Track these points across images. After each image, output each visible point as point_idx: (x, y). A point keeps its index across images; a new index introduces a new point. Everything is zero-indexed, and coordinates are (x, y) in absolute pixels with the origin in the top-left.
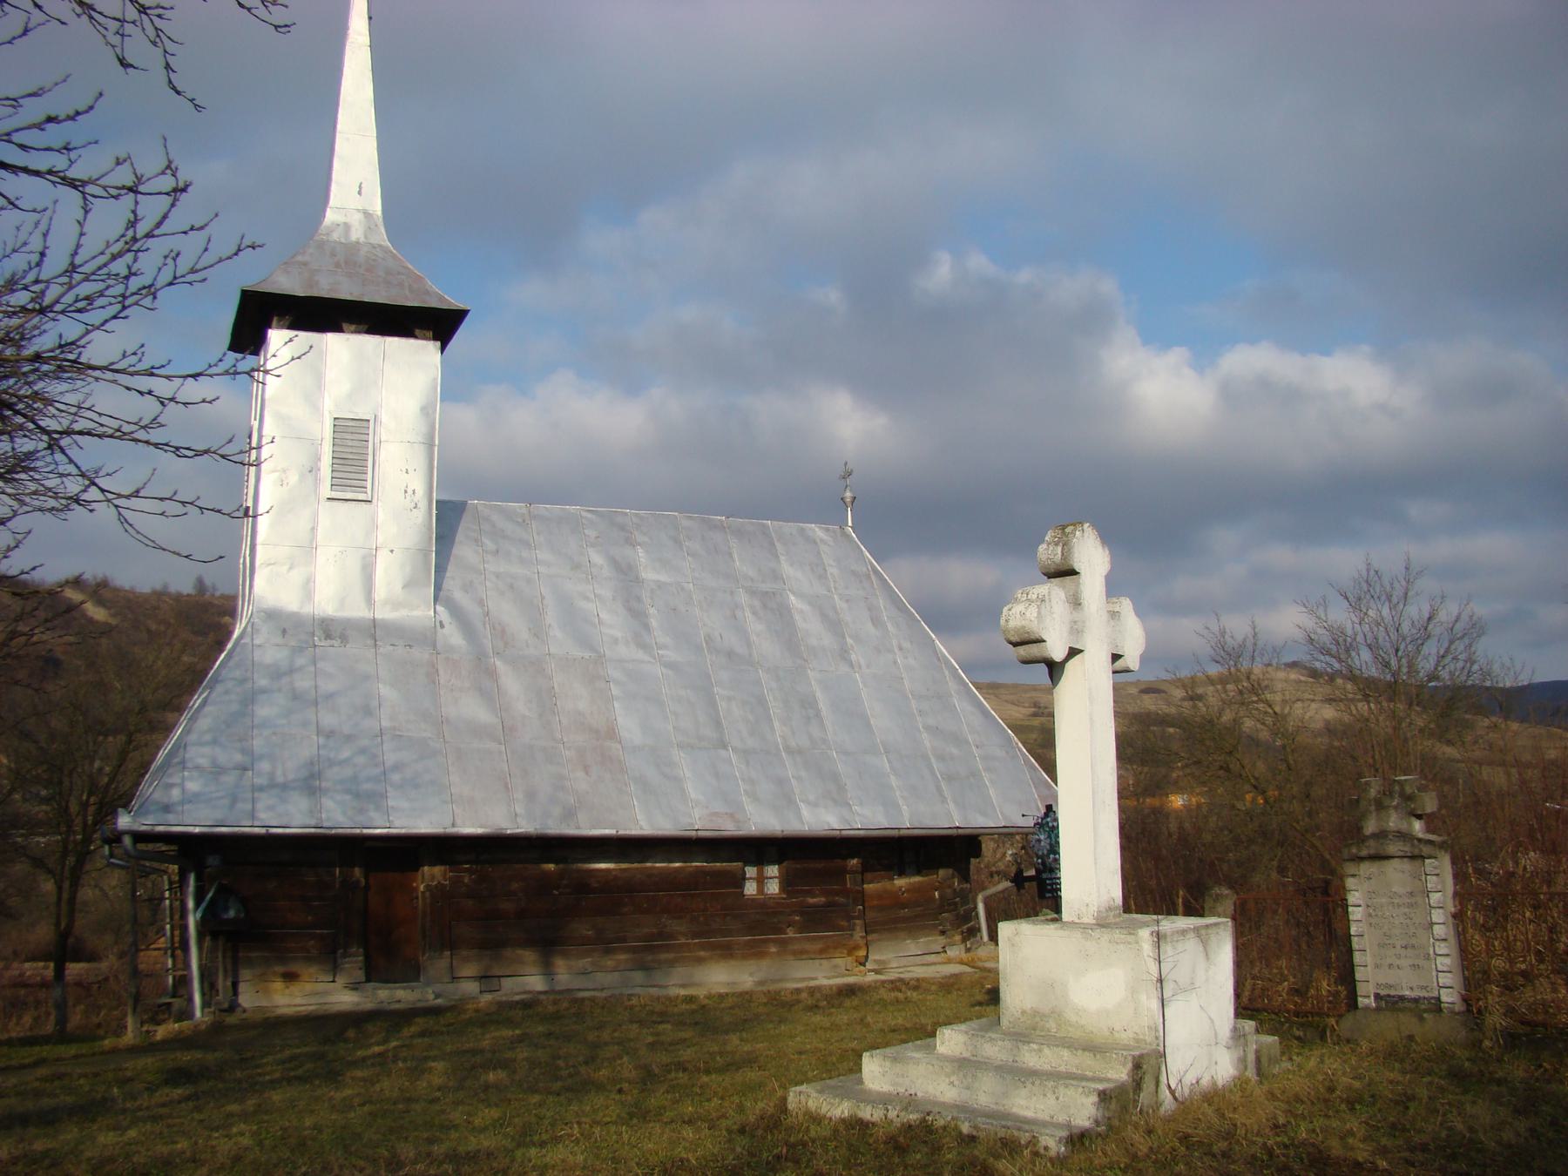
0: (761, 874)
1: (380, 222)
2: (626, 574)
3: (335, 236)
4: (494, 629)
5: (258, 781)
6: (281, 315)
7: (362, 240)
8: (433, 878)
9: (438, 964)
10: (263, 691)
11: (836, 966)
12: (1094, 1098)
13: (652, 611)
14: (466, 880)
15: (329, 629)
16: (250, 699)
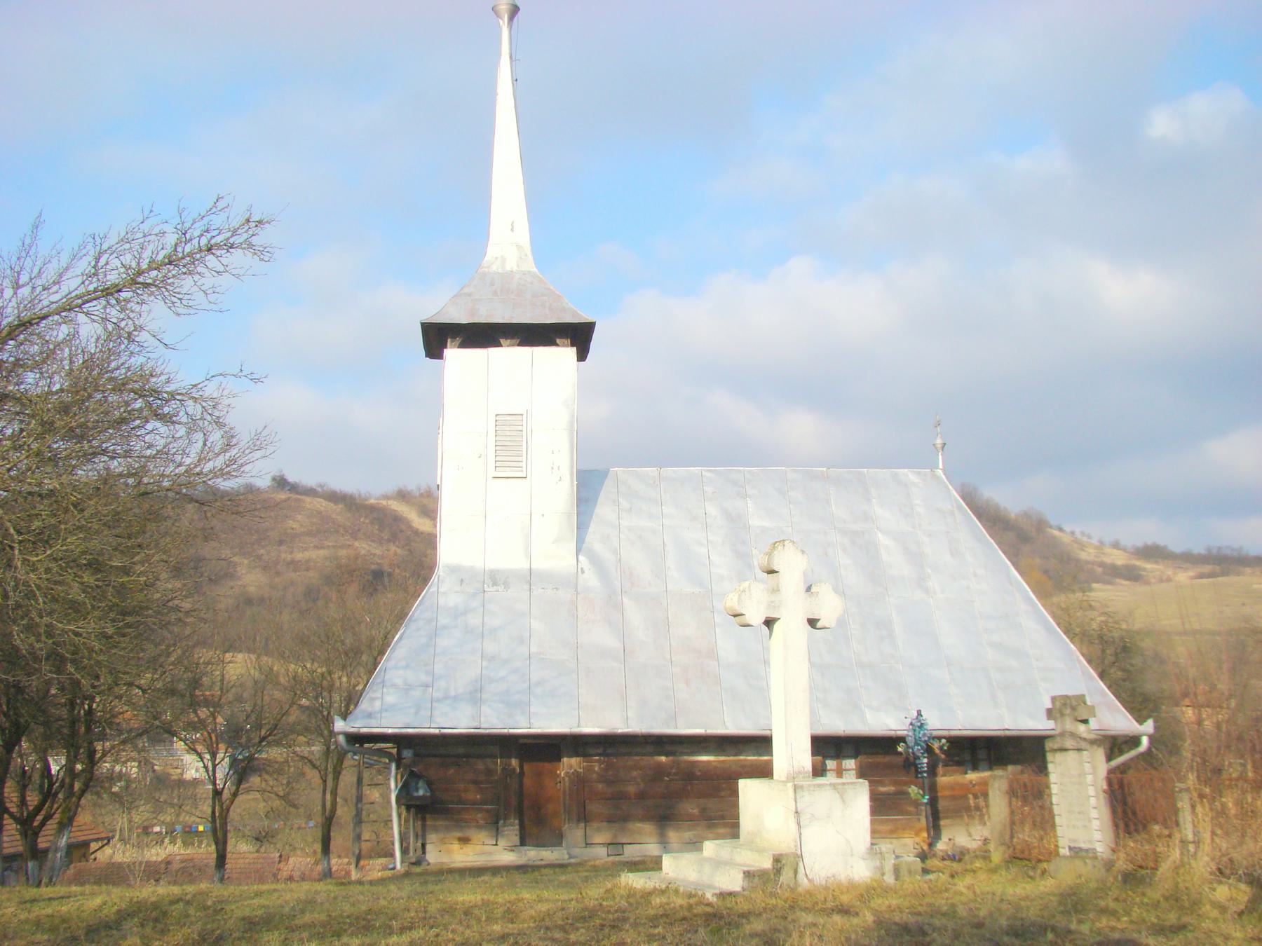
0: (839, 766)
1: (529, 252)
2: (736, 522)
3: (494, 268)
4: (624, 572)
5: (436, 695)
6: (454, 338)
7: (515, 269)
8: (571, 767)
9: (574, 833)
10: (444, 627)
11: (905, 845)
12: (741, 875)
13: (755, 552)
14: (596, 769)
15: (495, 578)
16: (435, 634)
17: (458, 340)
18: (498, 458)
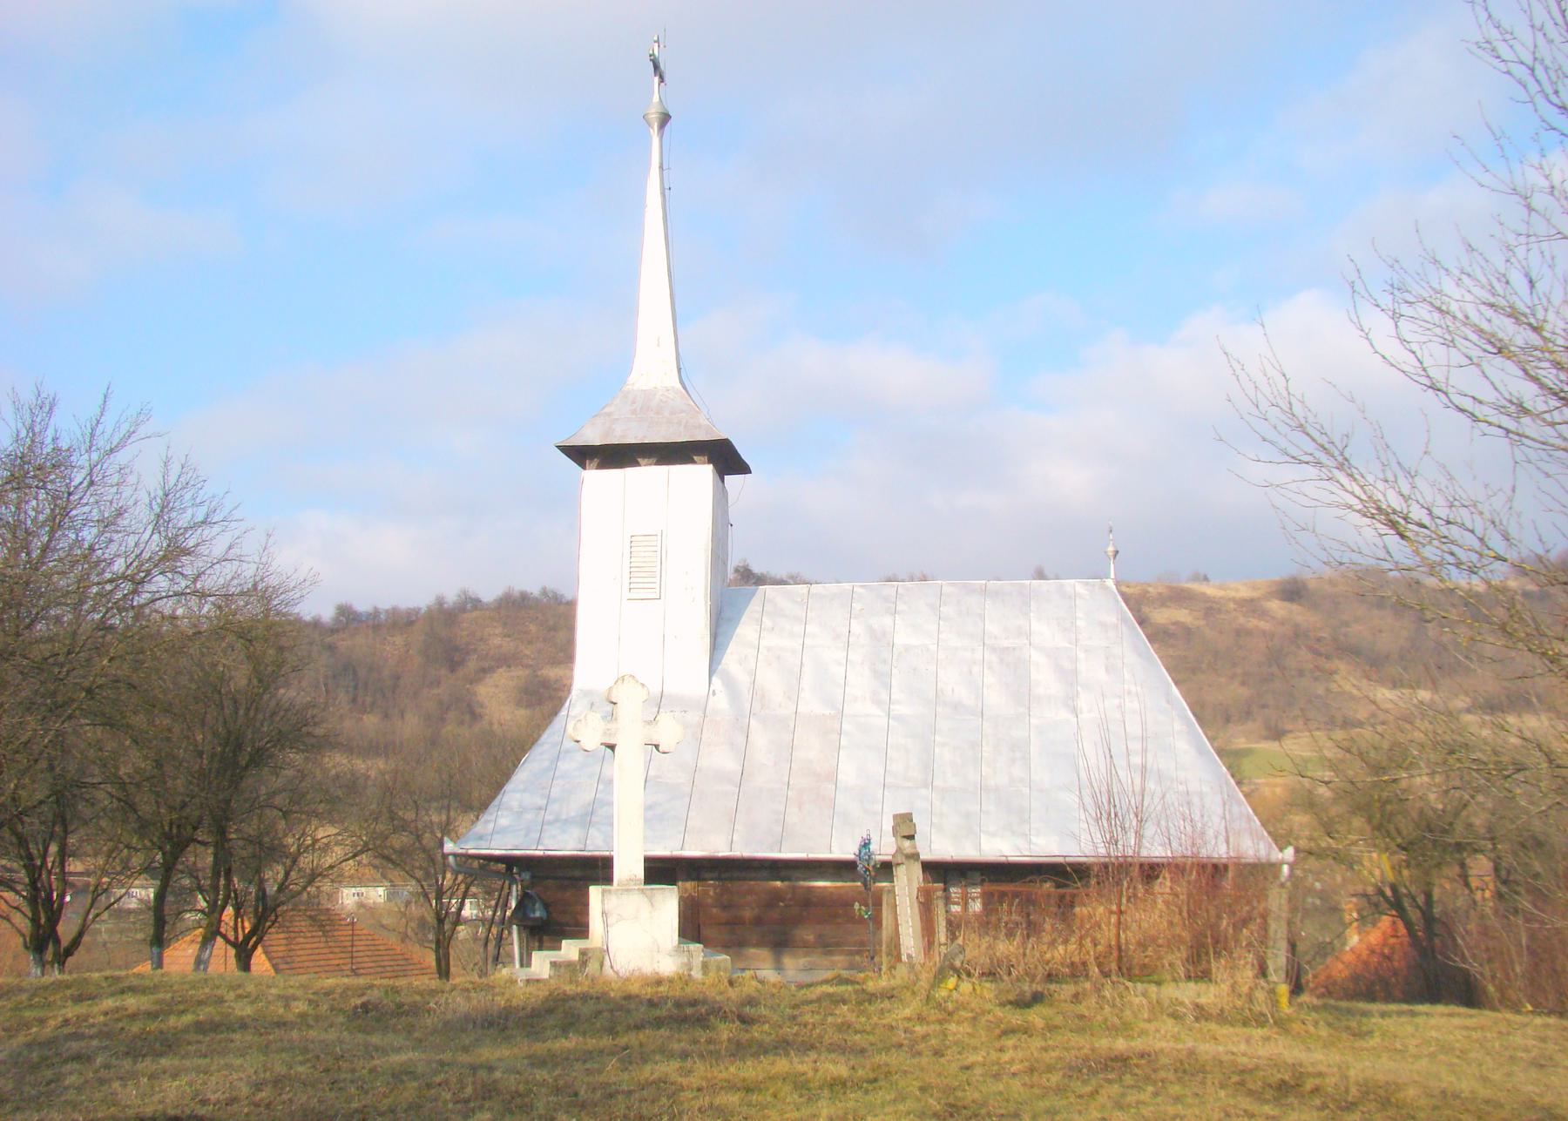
6: (591, 459)
14: (711, 893)
17: (596, 461)
18: (632, 580)
